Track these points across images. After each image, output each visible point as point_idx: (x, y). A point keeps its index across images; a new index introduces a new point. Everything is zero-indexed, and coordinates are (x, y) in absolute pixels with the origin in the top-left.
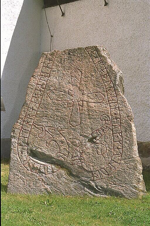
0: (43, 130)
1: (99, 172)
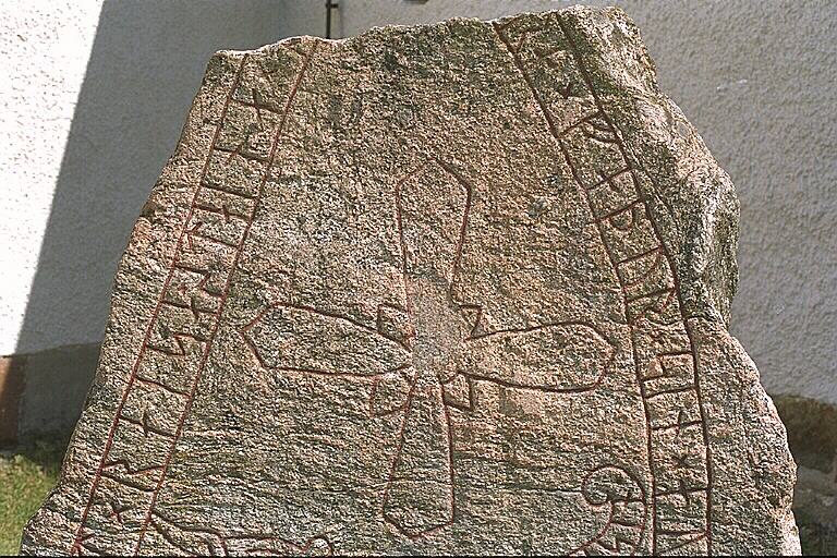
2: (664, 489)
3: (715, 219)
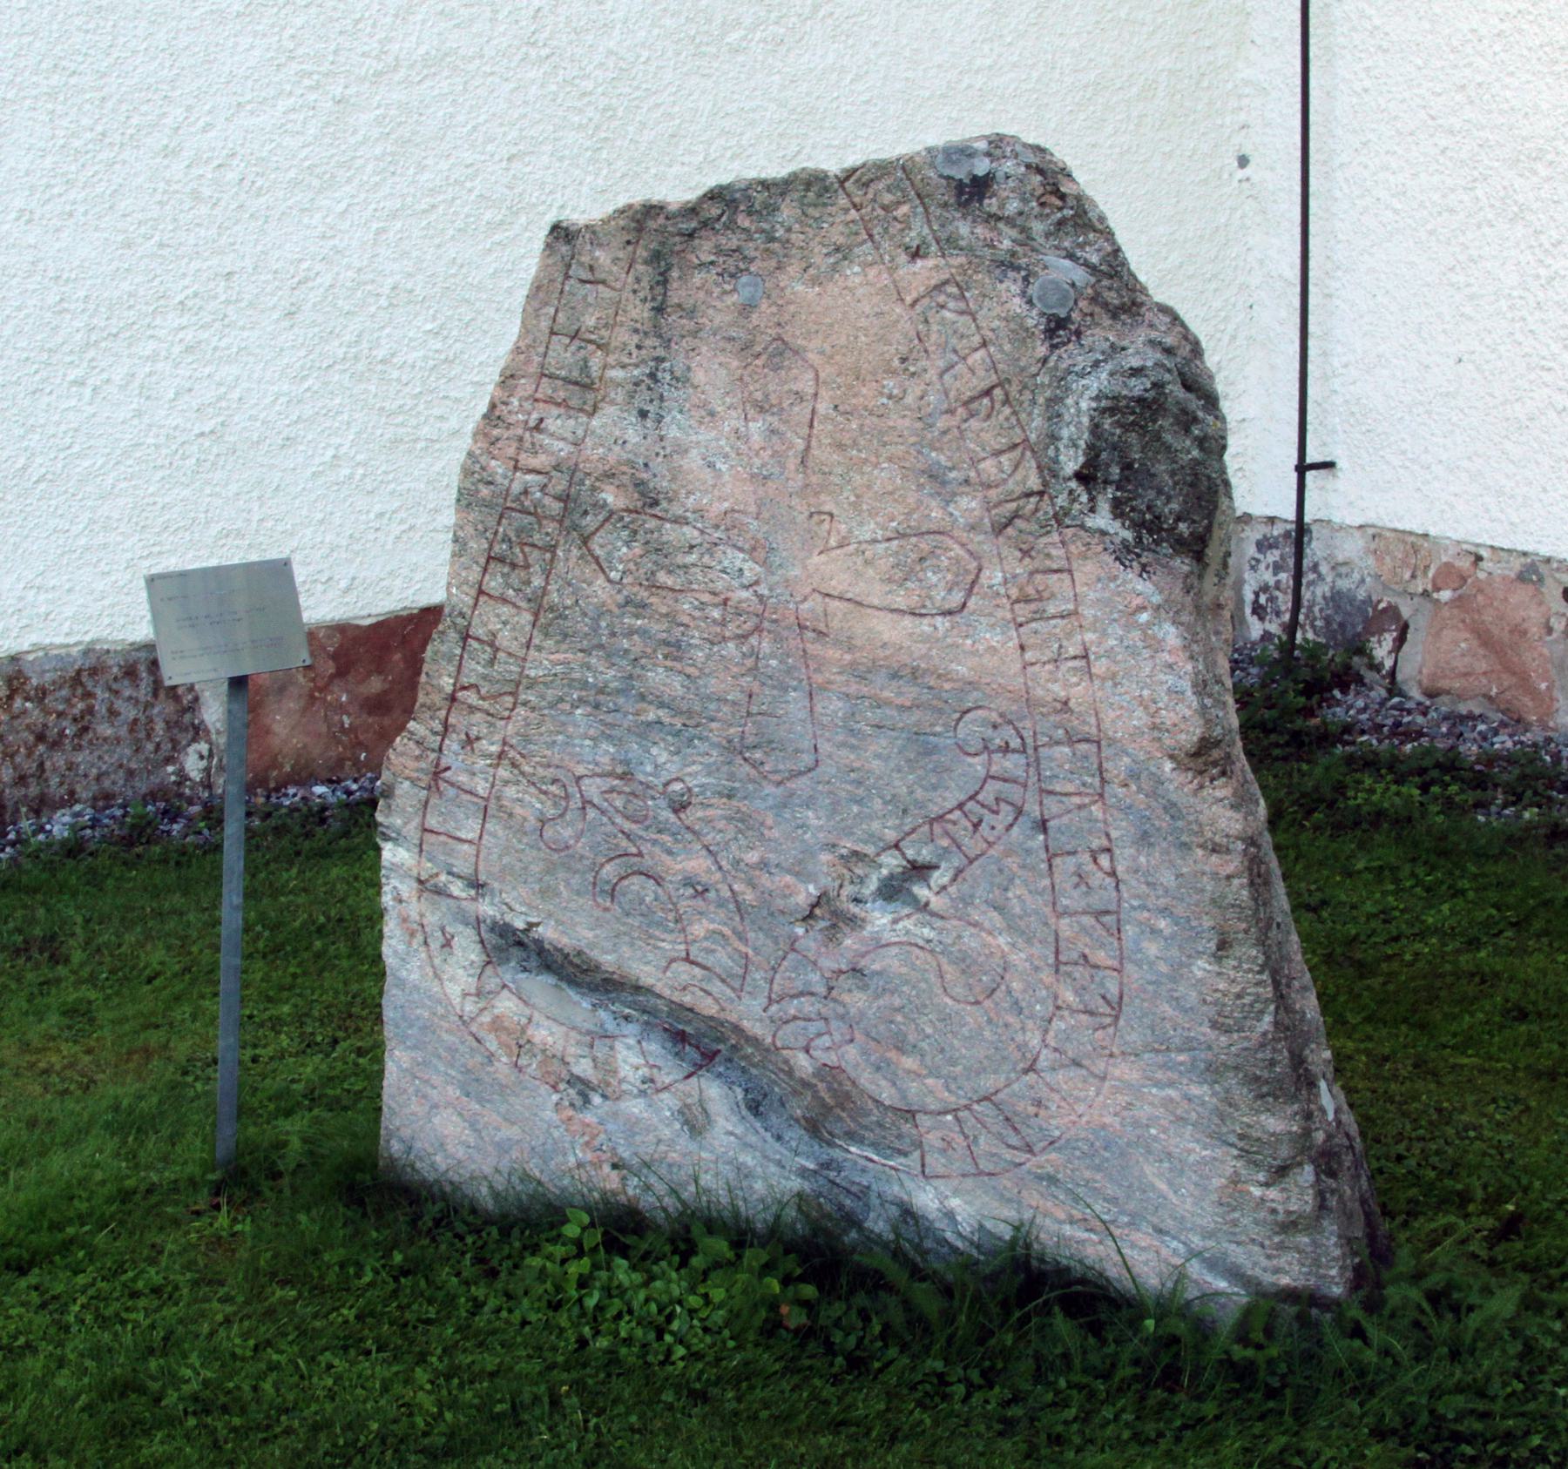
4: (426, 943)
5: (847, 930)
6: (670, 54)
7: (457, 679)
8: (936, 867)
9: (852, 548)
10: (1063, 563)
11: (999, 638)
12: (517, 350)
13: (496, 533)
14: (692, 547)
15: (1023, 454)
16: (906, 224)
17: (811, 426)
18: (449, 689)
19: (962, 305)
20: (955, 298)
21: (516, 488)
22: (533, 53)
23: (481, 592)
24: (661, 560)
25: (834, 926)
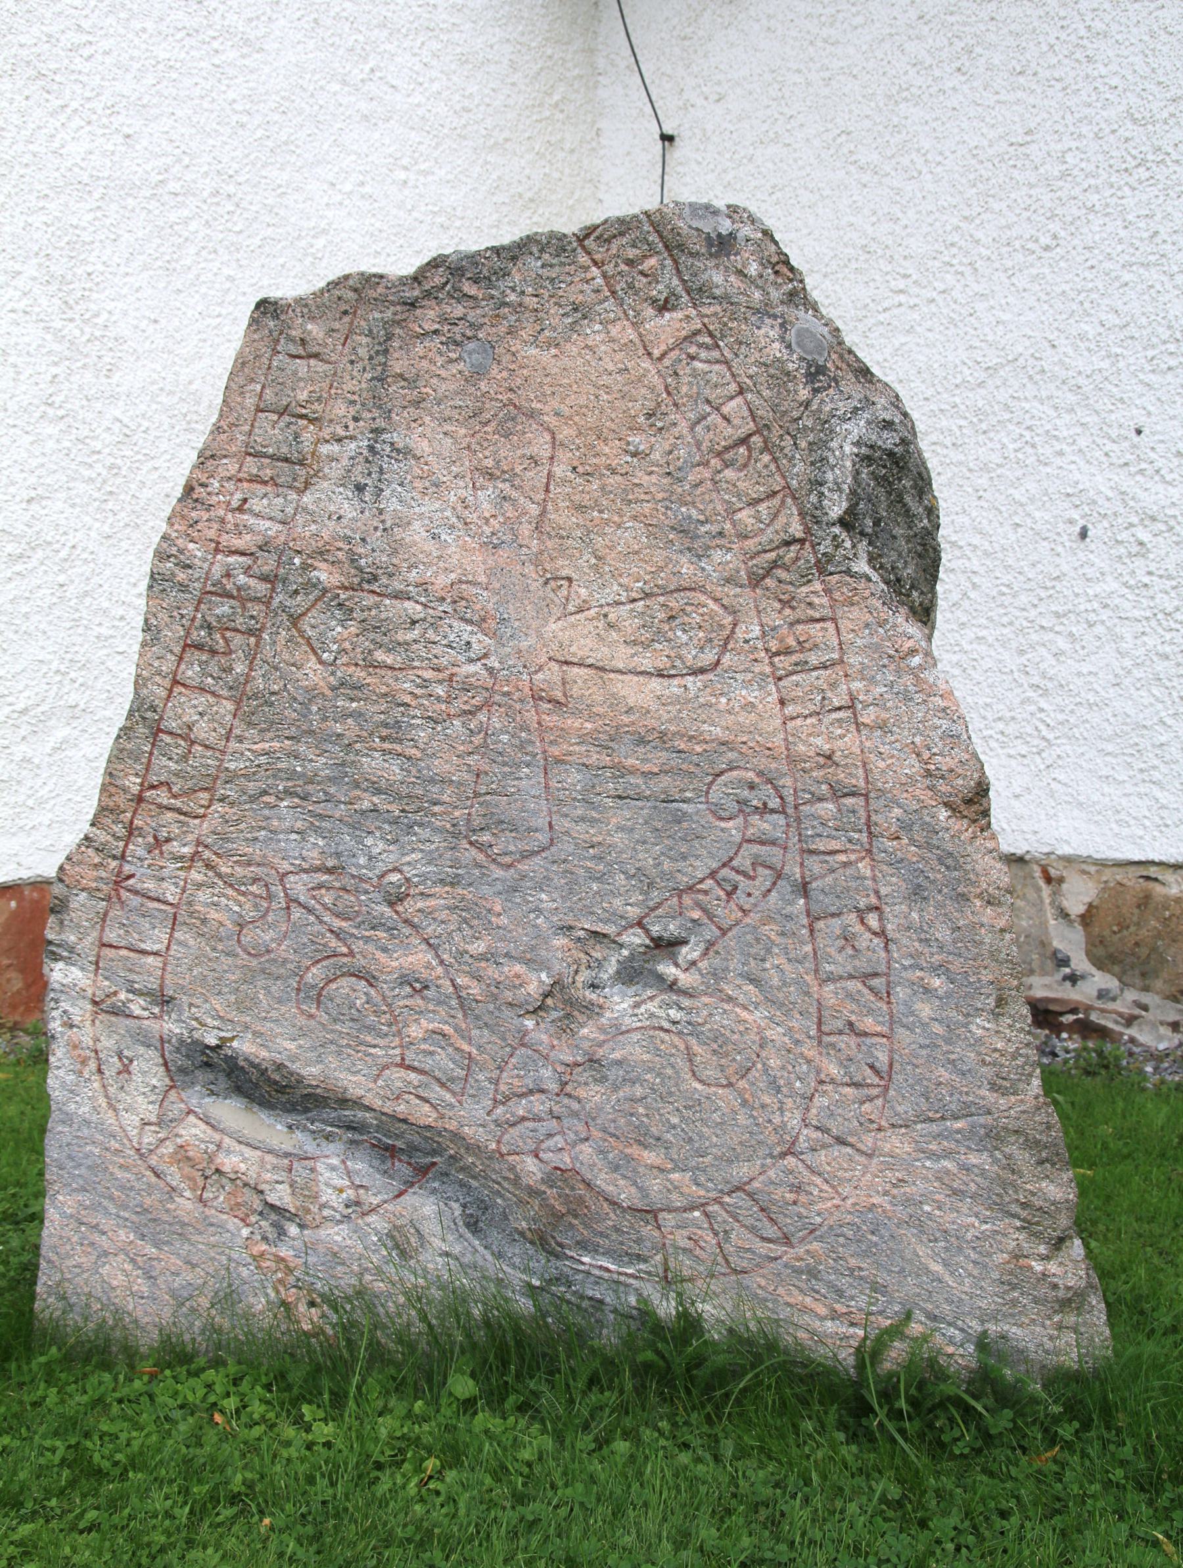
0: (270, 897)
1: (706, 1214)
2: (808, 796)
3: (855, 450)
4: (100, 1071)
5: (581, 1018)
6: (166, 427)
7: (144, 777)
8: (685, 942)
9: (592, 612)
10: (827, 612)
11: (756, 693)
12: (217, 429)
13: (193, 620)
14: (414, 622)
15: (783, 502)
16: (651, 277)
17: (547, 491)
18: (135, 789)
19: (716, 354)
20: (707, 348)
21: (217, 571)
22: (51, 411)
23: (176, 682)
24: (379, 638)
25: (568, 1016)
